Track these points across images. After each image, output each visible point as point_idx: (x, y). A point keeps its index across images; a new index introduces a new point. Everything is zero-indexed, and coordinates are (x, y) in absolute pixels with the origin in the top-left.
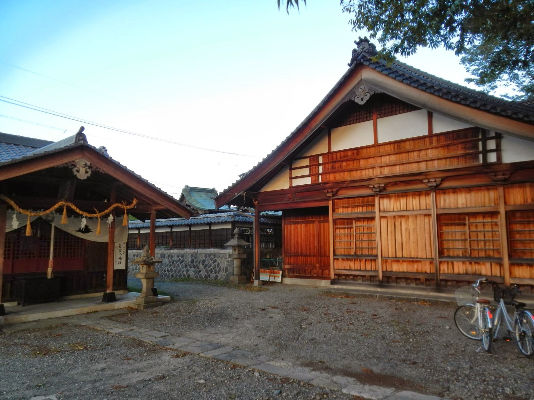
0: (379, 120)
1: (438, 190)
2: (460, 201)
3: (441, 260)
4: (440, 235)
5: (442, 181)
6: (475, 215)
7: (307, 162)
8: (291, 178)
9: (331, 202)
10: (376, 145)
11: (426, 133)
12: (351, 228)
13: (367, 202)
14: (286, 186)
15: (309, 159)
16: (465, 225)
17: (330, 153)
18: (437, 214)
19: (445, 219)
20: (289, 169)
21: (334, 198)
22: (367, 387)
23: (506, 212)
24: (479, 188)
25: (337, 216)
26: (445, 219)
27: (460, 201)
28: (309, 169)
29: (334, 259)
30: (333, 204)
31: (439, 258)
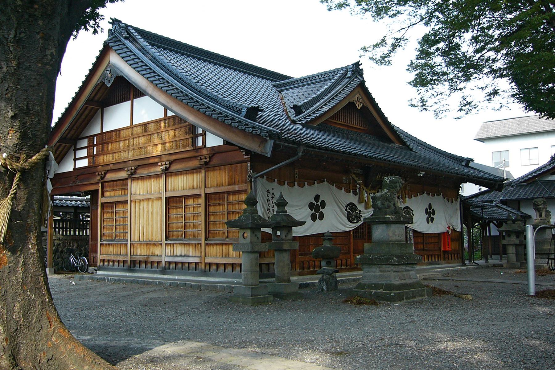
0: (135, 101)
1: (167, 172)
2: (181, 184)
3: (166, 242)
4: (167, 217)
5: (170, 164)
6: (187, 197)
7: (85, 143)
8: (75, 159)
9: (100, 185)
10: (132, 126)
11: (162, 116)
12: (113, 212)
13: (123, 183)
14: (71, 169)
15: (87, 140)
16: (181, 207)
17: (102, 133)
18: (166, 198)
19: (171, 202)
20: (74, 150)
21: (102, 181)
22: (544, 288)
23: (206, 194)
24: (198, 170)
25: (104, 200)
26: (171, 202)
27: (181, 184)
28: (86, 150)
29: (101, 244)
30: (103, 188)
31: (166, 240)
